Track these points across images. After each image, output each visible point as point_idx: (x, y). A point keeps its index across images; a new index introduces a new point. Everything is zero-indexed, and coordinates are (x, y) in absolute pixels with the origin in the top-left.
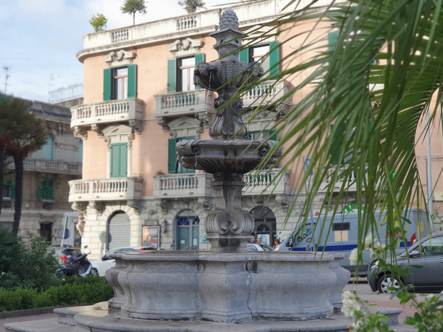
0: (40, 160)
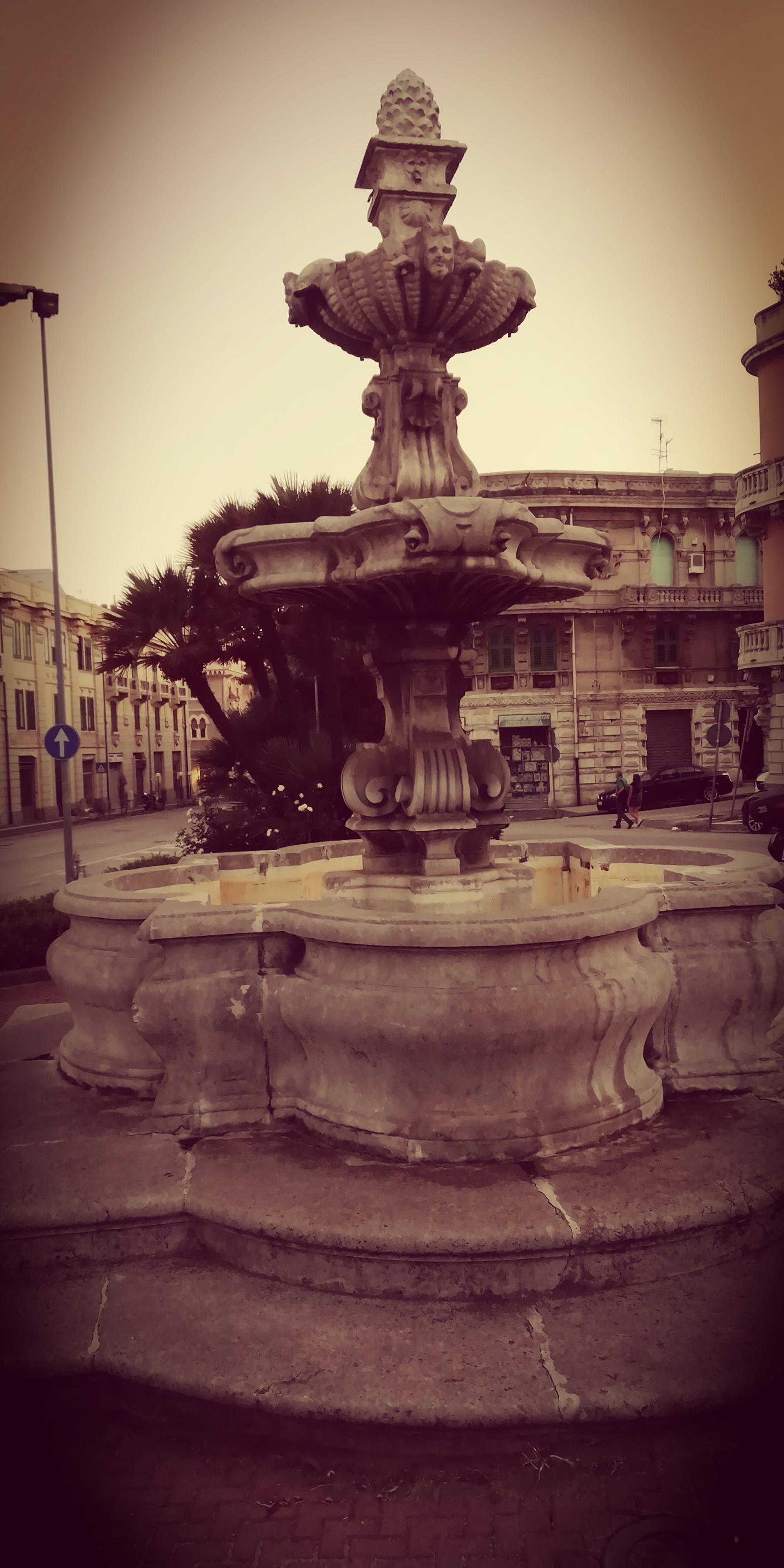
0: (731, 589)
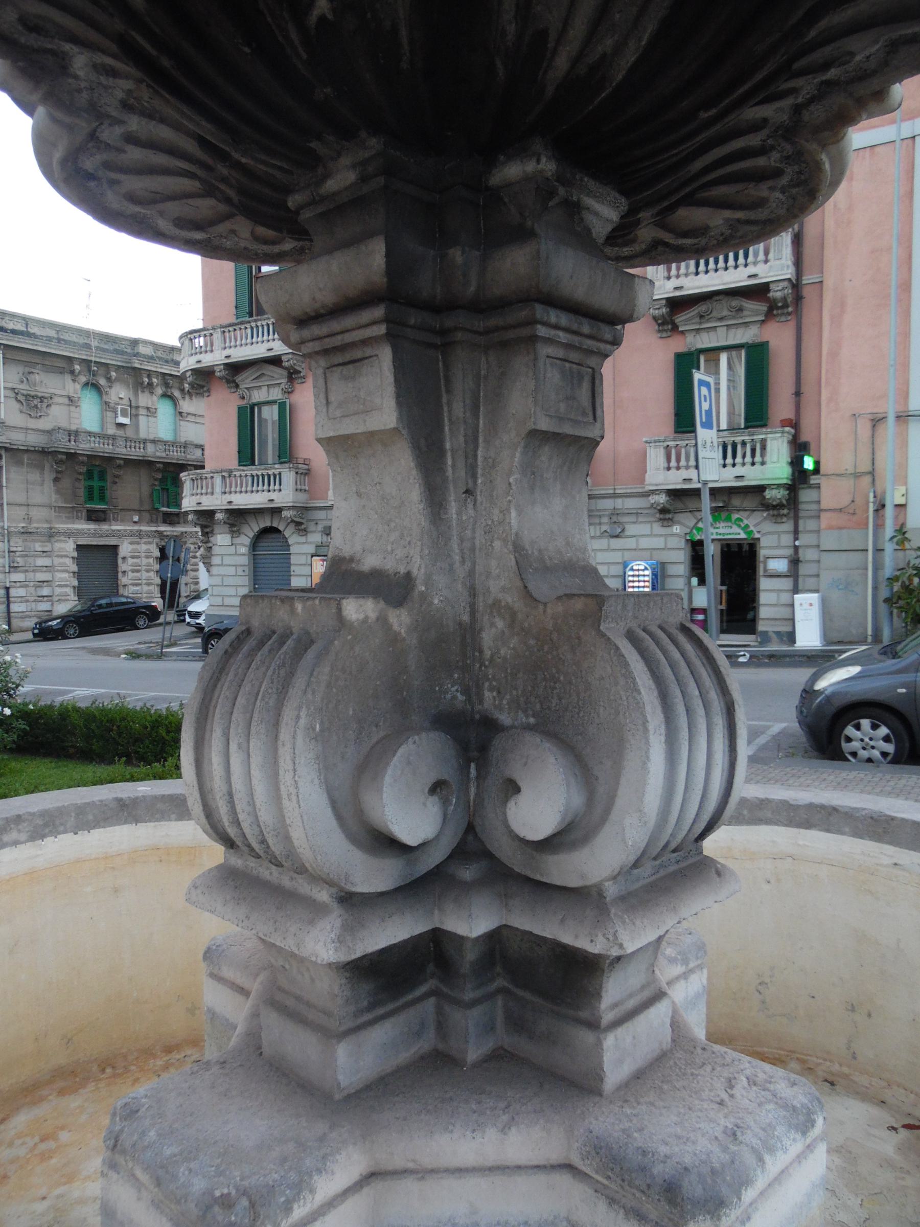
0: (154, 441)
